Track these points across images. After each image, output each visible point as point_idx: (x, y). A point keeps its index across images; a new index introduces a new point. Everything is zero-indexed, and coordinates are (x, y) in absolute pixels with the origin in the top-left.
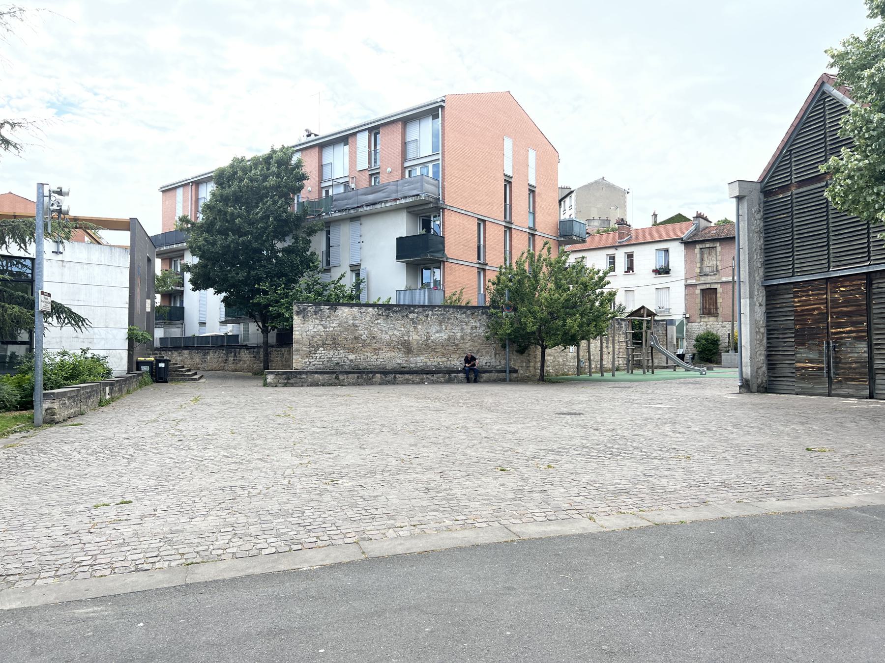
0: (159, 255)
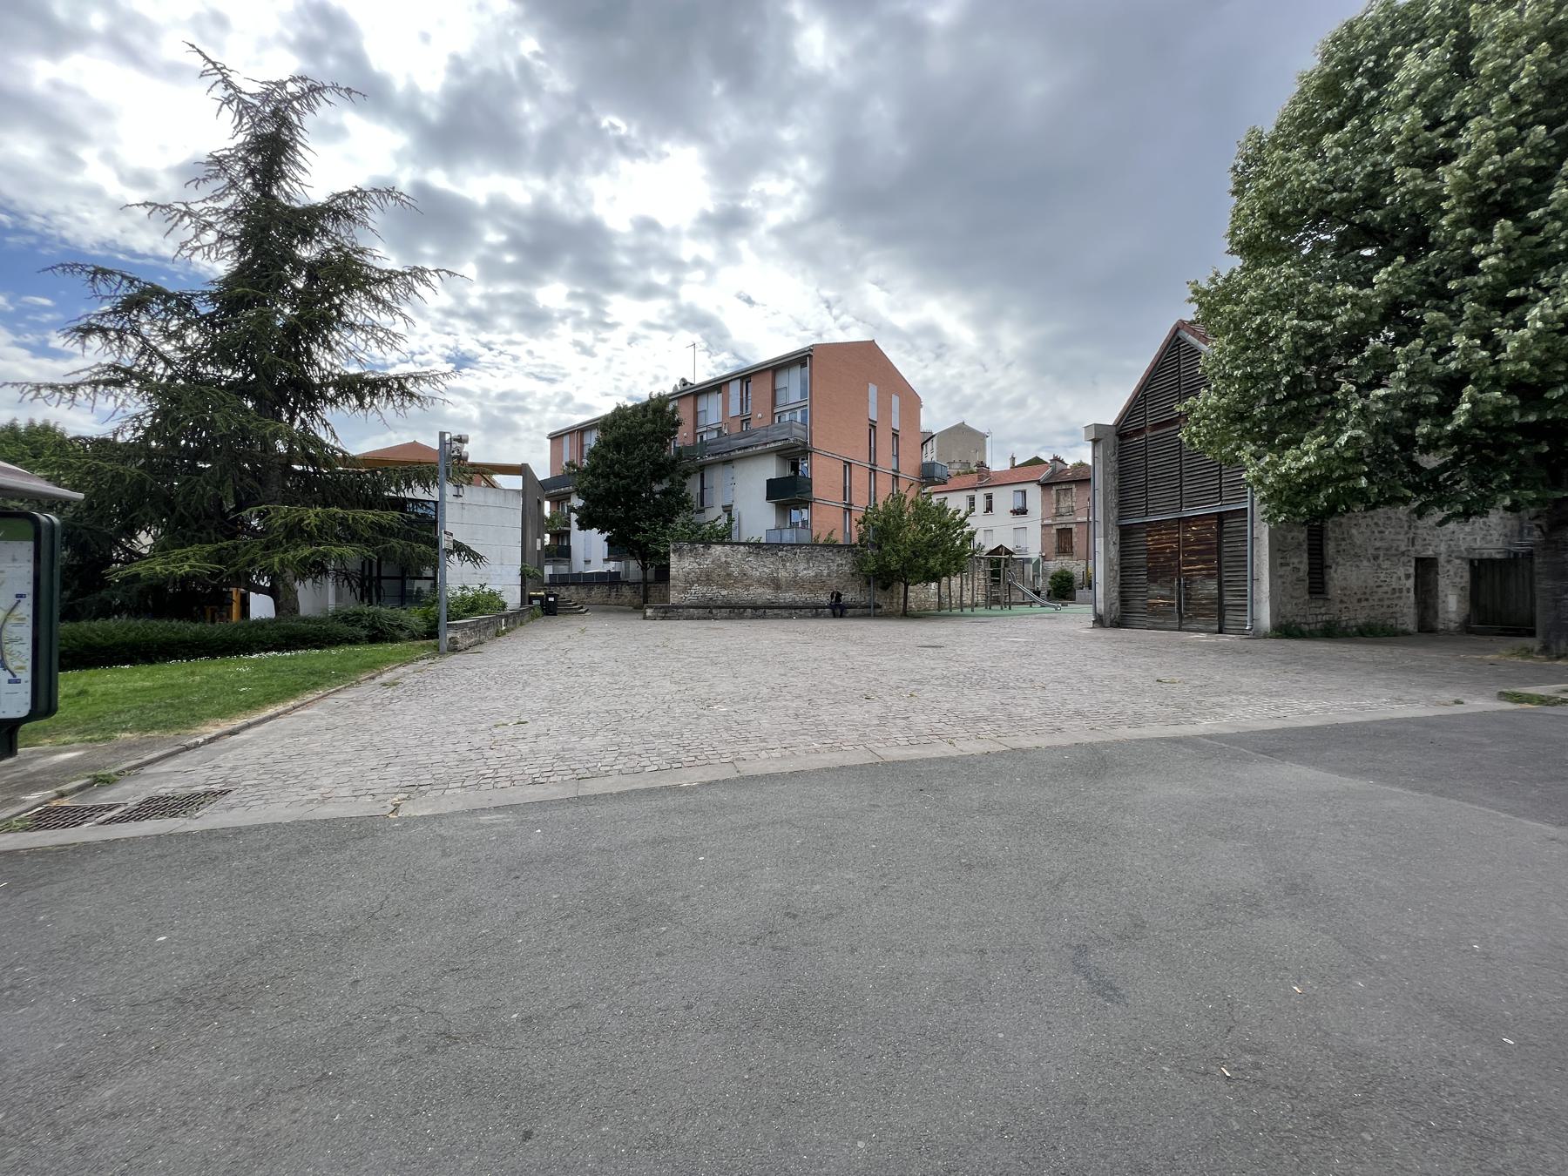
0: (548, 498)
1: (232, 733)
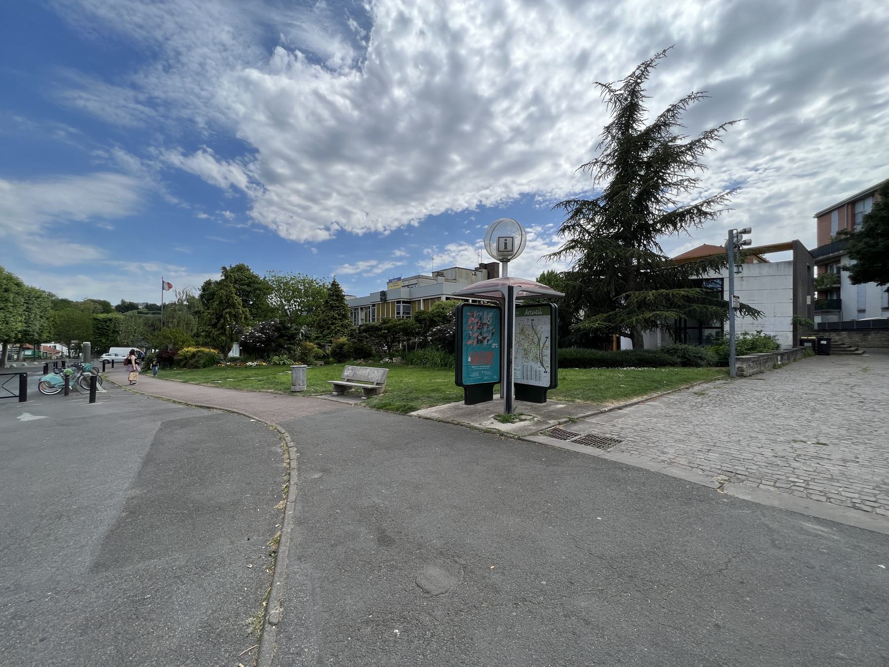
0: (817, 263)
1: (620, 408)
